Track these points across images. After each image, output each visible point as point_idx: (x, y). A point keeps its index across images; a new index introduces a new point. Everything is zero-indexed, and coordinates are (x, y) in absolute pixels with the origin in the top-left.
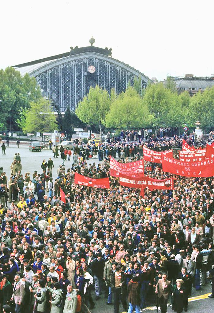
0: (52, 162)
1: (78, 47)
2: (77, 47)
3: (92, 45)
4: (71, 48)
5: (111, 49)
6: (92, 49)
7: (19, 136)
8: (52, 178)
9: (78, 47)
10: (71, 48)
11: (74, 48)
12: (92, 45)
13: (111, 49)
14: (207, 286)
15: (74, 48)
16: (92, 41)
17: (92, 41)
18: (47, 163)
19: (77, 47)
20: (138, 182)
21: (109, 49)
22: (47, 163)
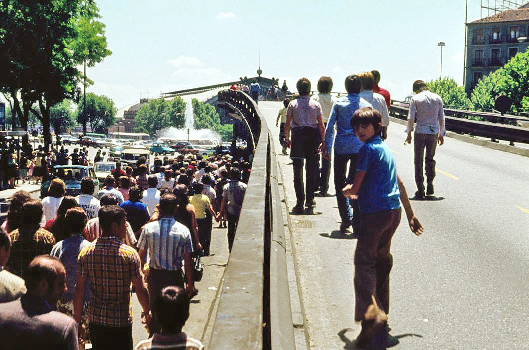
0: (414, 90)
1: (248, 78)
2: (246, 77)
3: (260, 75)
4: (241, 78)
5: (278, 80)
6: (260, 80)
7: (50, 194)
8: (106, 35)
9: (248, 78)
10: (241, 78)
11: (243, 78)
12: (260, 75)
13: (278, 80)
14: (57, 270)
15: (243, 78)
16: (260, 72)
17: (260, 72)
18: (473, 90)
19: (246, 77)
20: (420, 230)
21: (275, 79)
22: (473, 90)
